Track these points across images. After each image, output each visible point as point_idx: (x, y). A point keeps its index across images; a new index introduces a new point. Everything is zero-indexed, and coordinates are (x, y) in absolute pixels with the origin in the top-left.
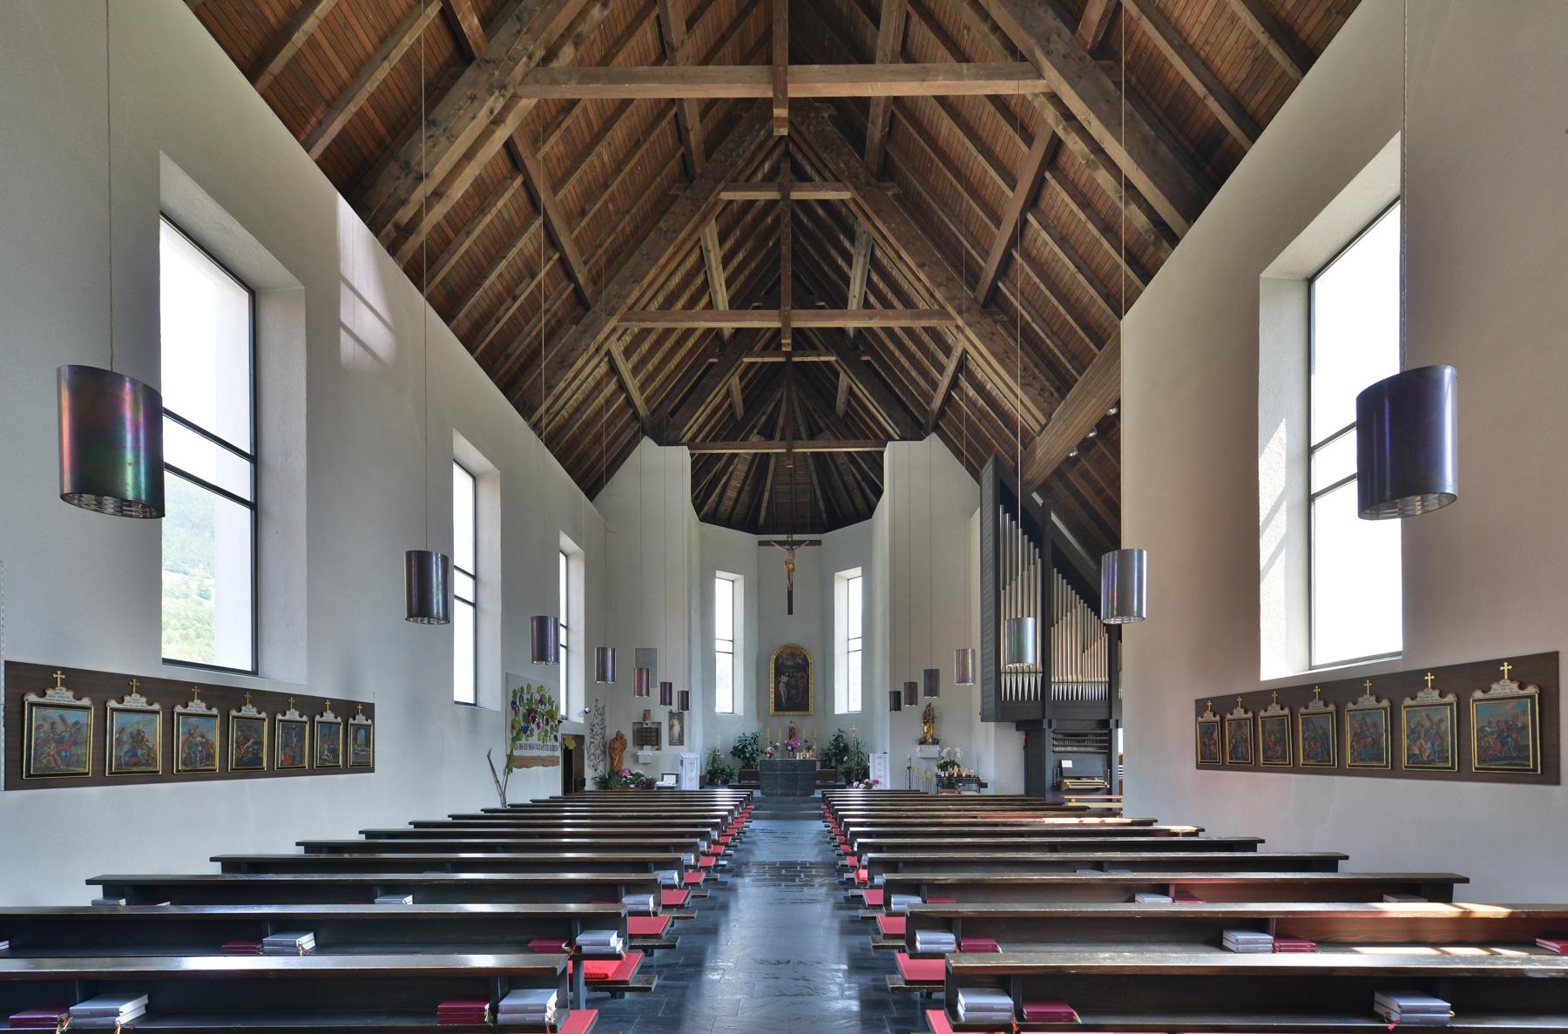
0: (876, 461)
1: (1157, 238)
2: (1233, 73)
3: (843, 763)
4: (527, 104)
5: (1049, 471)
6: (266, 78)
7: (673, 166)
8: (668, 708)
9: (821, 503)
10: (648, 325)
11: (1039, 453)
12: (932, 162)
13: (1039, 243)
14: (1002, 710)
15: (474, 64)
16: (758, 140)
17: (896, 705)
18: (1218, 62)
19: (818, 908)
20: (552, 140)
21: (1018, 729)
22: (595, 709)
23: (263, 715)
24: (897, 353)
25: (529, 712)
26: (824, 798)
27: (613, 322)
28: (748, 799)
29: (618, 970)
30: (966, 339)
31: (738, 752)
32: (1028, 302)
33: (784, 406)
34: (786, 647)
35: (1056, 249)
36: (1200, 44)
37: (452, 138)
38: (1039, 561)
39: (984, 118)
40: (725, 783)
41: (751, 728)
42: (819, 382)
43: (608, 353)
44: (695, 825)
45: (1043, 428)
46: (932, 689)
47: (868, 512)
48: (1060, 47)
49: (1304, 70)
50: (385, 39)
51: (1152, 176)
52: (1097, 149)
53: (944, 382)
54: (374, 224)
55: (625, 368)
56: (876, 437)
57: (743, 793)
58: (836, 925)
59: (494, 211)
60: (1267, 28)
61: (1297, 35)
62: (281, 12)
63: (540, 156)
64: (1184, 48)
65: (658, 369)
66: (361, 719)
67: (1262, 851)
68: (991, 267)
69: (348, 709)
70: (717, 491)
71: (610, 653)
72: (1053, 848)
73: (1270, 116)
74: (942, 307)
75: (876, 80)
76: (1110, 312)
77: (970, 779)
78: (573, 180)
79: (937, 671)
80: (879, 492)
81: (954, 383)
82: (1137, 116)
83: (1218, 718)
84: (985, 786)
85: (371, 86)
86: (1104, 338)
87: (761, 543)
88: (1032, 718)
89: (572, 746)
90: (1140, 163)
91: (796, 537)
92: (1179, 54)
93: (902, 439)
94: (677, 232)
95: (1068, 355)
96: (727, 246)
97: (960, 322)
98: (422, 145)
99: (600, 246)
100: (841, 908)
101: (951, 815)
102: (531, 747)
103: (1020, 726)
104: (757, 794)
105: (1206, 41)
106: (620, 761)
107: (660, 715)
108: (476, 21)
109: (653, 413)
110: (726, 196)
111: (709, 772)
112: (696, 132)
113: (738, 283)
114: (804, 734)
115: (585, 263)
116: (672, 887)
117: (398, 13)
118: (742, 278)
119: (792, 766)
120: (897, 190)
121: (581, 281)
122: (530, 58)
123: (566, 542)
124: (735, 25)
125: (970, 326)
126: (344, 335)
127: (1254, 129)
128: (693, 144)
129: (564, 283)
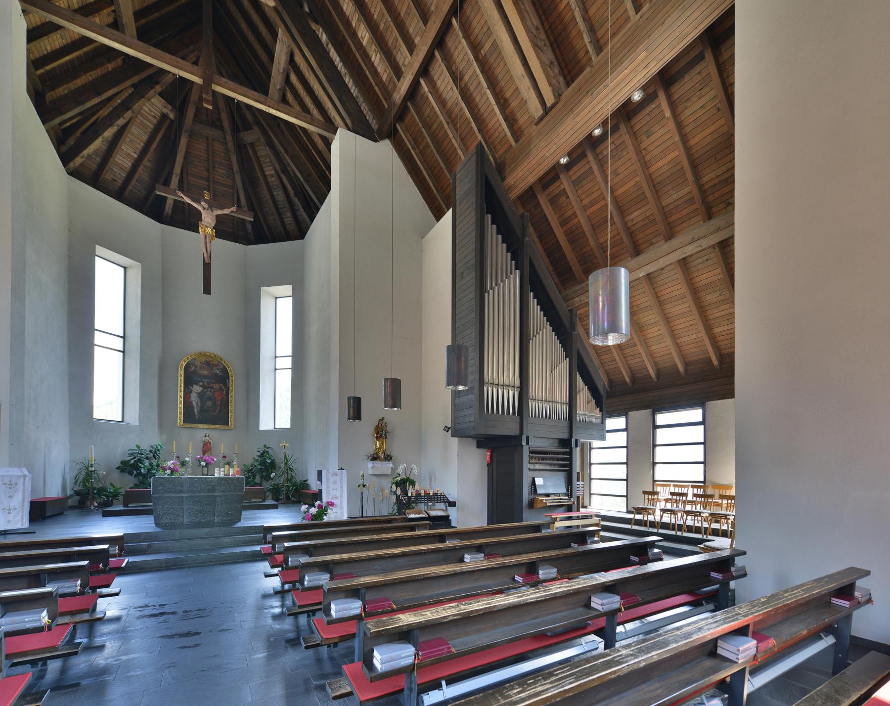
21: (479, 446)
31: (129, 467)
34: (200, 354)
81: (424, 70)
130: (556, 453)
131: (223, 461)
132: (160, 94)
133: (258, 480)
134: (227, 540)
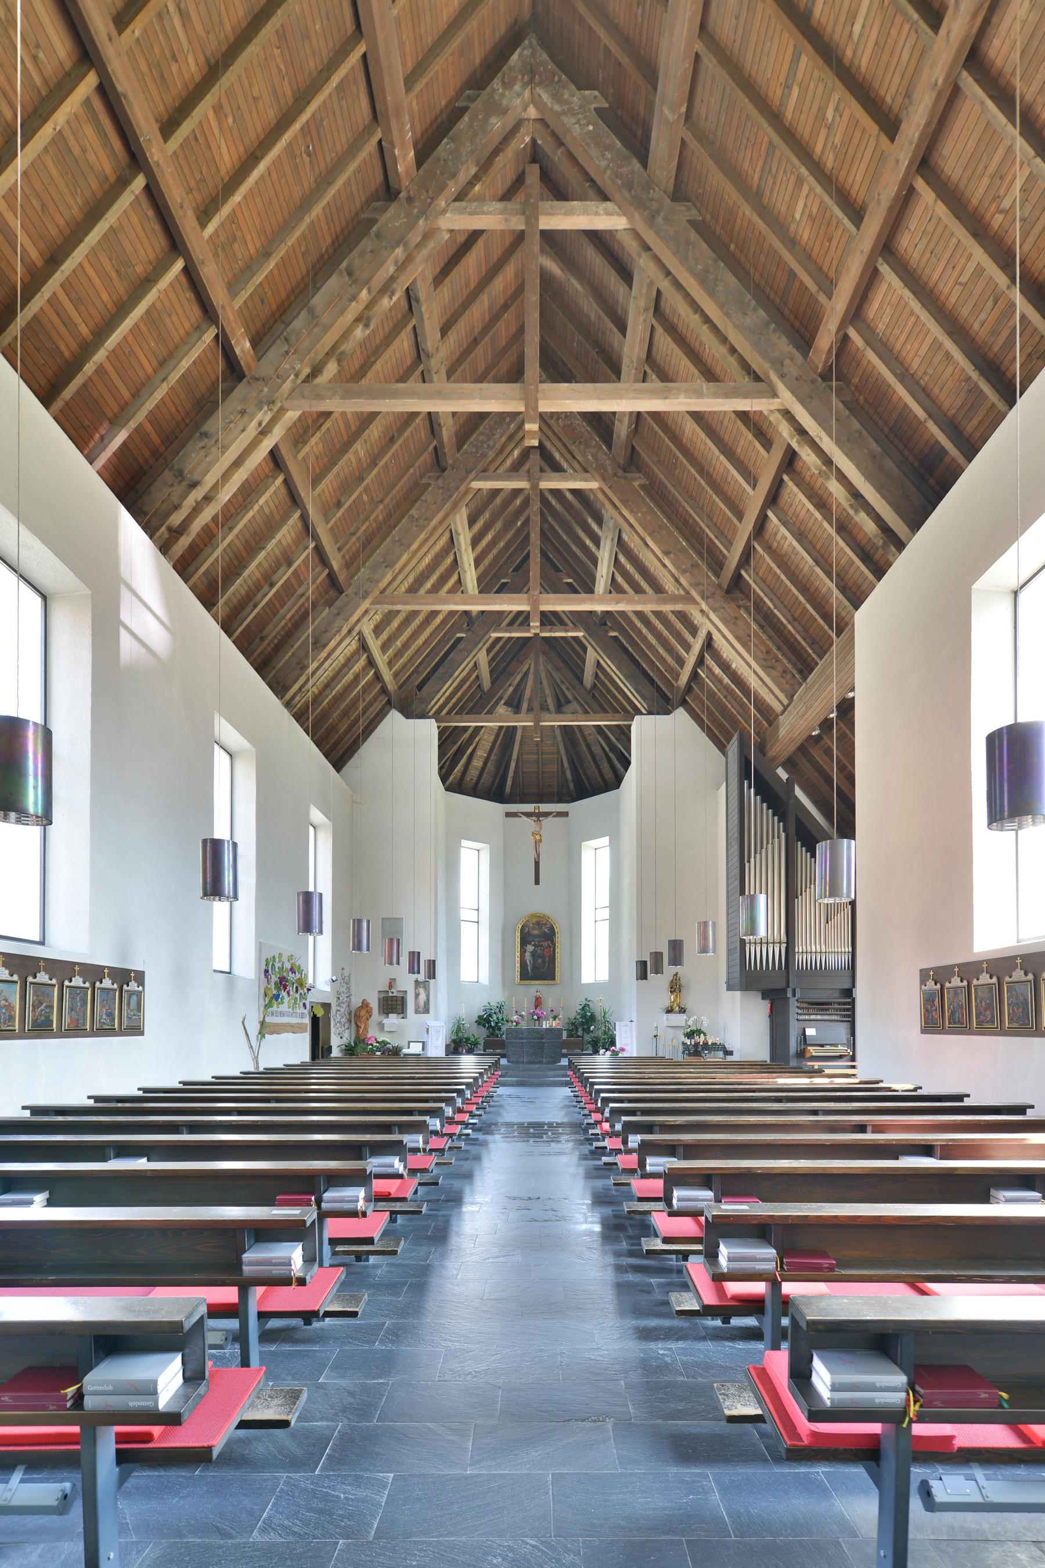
0: (624, 734)
1: (885, 543)
2: (950, 400)
3: (589, 1031)
4: (292, 415)
5: (792, 749)
6: (58, 404)
7: (427, 457)
8: (416, 976)
9: (568, 774)
10: (398, 607)
11: (782, 732)
12: (677, 458)
13: (779, 537)
14: (749, 978)
15: (245, 381)
16: (508, 433)
17: (643, 975)
18: (936, 390)
19: (564, 1159)
20: (313, 441)
22: (342, 979)
23: (54, 981)
24: (644, 631)
25: (281, 980)
26: (571, 1066)
27: (365, 605)
28: (496, 1065)
29: (398, 1189)
30: (710, 621)
31: (483, 1021)
32: (772, 590)
33: (531, 677)
34: (533, 916)
35: (795, 543)
36: (920, 374)
37: (225, 448)
38: (783, 835)
39: (726, 422)
40: (470, 1052)
41: (495, 997)
42: (568, 656)
43: (360, 633)
44: (409, 1112)
45: (785, 708)
46: (676, 959)
47: (616, 782)
48: (793, 371)
49: (879, 579)
50: (164, 363)
51: (879, 488)
52: (828, 461)
53: (691, 660)
54: (149, 529)
55: (374, 645)
56: (625, 710)
57: (492, 1059)
58: (581, 1171)
59: (256, 508)
60: (977, 367)
61: (1004, 373)
62: (74, 346)
63: (300, 456)
64: (905, 376)
65: (406, 645)
66: (133, 986)
67: (967, 1102)
68: (733, 557)
69: (123, 976)
70: (465, 757)
71: (365, 925)
72: (779, 1100)
73: (985, 440)
74: (687, 592)
75: (621, 398)
76: (847, 603)
77: (715, 1047)
78: (331, 476)
79: (681, 942)
80: (626, 763)
81: (700, 662)
82: (864, 432)
83: (938, 986)
84: (731, 1053)
85: (150, 405)
86: (844, 626)
87: (508, 815)
88: (774, 985)
89: (320, 1013)
90: (868, 477)
91: (544, 807)
92: (901, 381)
93: (650, 713)
94: (429, 520)
95: (805, 643)
96: (477, 527)
97: (704, 606)
98: (192, 458)
99: (354, 534)
100: (585, 1159)
101: (691, 1076)
102: (282, 1014)
103: (766, 995)
104: (503, 1062)
105: (925, 373)
106: (366, 1029)
107: (406, 983)
108: (248, 344)
109: (400, 687)
110: (476, 485)
111: (454, 1041)
112: (447, 432)
113: (486, 562)
114: (550, 1003)
115: (339, 549)
116: (415, 1150)
117: (176, 339)
118: (490, 557)
119: (538, 1039)
120: (643, 481)
121: (335, 565)
122: (297, 375)
123: (316, 815)
124: (487, 328)
125: (714, 610)
126: (124, 634)
127: (971, 450)
128: (445, 438)
129: (319, 569)
130: (840, 1004)
131: (551, 1015)
132: (505, 704)
133: (580, 1033)
134: (550, 1073)
